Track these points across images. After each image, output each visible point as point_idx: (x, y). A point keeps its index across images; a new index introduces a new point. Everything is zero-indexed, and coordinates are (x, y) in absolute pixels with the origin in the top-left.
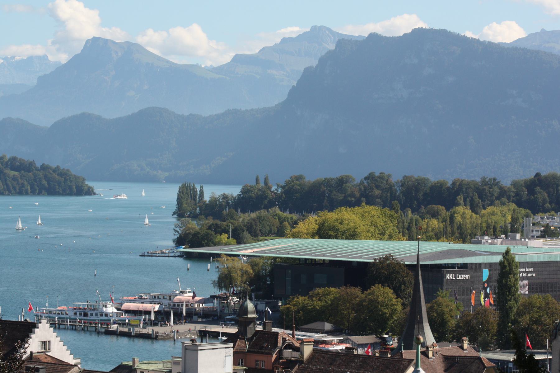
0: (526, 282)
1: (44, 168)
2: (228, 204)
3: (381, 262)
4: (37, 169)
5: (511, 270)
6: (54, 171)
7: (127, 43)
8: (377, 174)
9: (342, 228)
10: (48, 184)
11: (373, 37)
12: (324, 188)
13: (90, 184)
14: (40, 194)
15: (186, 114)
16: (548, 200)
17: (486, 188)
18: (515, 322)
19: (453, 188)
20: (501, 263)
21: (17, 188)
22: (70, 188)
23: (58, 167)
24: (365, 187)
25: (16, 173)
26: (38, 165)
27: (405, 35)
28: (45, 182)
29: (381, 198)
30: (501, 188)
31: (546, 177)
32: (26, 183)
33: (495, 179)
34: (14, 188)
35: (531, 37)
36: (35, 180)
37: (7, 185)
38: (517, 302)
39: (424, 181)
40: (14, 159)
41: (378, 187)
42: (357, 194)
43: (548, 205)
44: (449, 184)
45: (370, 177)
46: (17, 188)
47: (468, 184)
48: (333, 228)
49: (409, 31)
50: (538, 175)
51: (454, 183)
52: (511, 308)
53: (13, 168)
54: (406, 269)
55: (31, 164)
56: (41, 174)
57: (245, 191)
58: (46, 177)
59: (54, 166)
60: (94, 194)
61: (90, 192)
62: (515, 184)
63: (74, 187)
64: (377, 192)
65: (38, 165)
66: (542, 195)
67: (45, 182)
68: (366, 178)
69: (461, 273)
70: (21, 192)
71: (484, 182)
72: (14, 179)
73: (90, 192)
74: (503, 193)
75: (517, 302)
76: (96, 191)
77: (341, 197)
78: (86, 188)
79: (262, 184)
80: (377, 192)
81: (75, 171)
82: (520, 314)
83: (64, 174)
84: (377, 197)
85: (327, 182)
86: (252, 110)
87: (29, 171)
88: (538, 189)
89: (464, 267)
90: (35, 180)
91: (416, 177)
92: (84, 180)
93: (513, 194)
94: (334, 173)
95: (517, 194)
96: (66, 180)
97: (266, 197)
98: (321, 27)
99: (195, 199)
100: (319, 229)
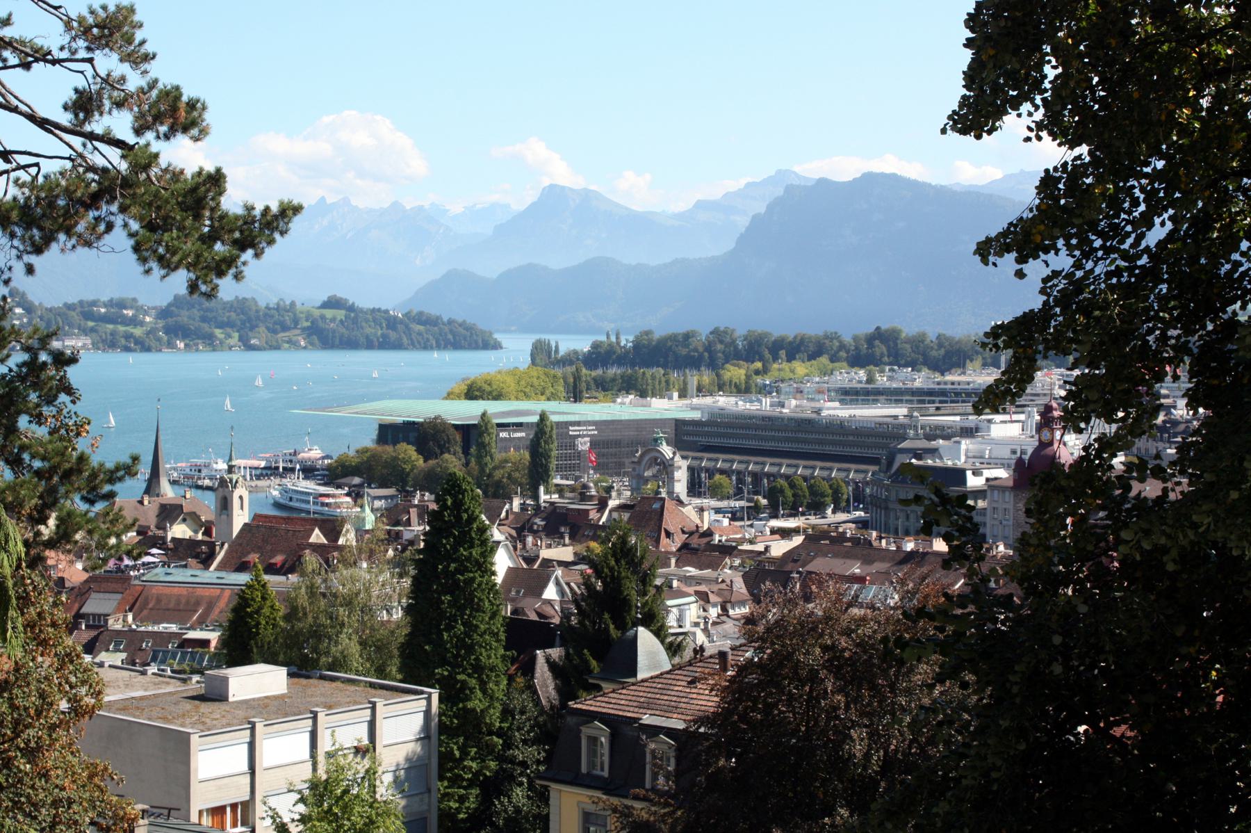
0: (587, 439)
1: (451, 322)
2: (578, 359)
3: (430, 422)
4: (444, 324)
5: (486, 429)
6: (460, 325)
7: (585, 189)
8: (722, 329)
9: (488, 388)
10: (454, 338)
11: (823, 183)
12: (670, 344)
13: (497, 336)
14: (445, 348)
15: (634, 263)
16: (886, 353)
17: (826, 341)
18: (490, 476)
19: (795, 342)
20: (538, 424)
21: (422, 342)
22: (476, 342)
23: (464, 321)
24: (709, 342)
25: (421, 328)
26: (445, 319)
27: (855, 180)
28: (450, 337)
29: (723, 353)
30: (840, 342)
31: (886, 331)
32: (431, 337)
33: (836, 333)
34: (419, 342)
35: (1007, 178)
36: (441, 335)
37: (412, 340)
38: (492, 458)
39: (766, 335)
40: (421, 313)
41: (721, 342)
42: (701, 349)
43: (886, 359)
44: (790, 339)
45: (715, 332)
46: (422, 342)
47: (810, 338)
48: (479, 389)
49: (858, 175)
50: (878, 328)
51: (795, 337)
52: (486, 464)
53: (420, 323)
54: (452, 430)
55: (438, 318)
56: (446, 329)
57: (596, 346)
58: (451, 331)
59: (460, 320)
60: (501, 348)
61: (497, 346)
62: (855, 338)
63: (480, 341)
64: (719, 347)
65: (445, 319)
66: (880, 348)
67: (450, 337)
68: (711, 333)
69: (515, 431)
70: (426, 347)
71: (826, 337)
72: (420, 334)
73: (497, 346)
74: (842, 346)
75: (492, 458)
76: (504, 345)
77: (684, 352)
78: (492, 342)
79: (613, 339)
80: (719, 347)
81: (482, 325)
82: (495, 468)
83: (470, 328)
84: (719, 351)
85: (673, 338)
86: (700, 259)
87: (435, 326)
88: (877, 342)
89: (520, 425)
90: (441, 335)
91: (759, 331)
92: (491, 334)
93: (853, 348)
94: (680, 328)
95: (857, 348)
96: (471, 334)
97: (614, 353)
98: (786, 170)
99: (550, 357)
100: (469, 390)
